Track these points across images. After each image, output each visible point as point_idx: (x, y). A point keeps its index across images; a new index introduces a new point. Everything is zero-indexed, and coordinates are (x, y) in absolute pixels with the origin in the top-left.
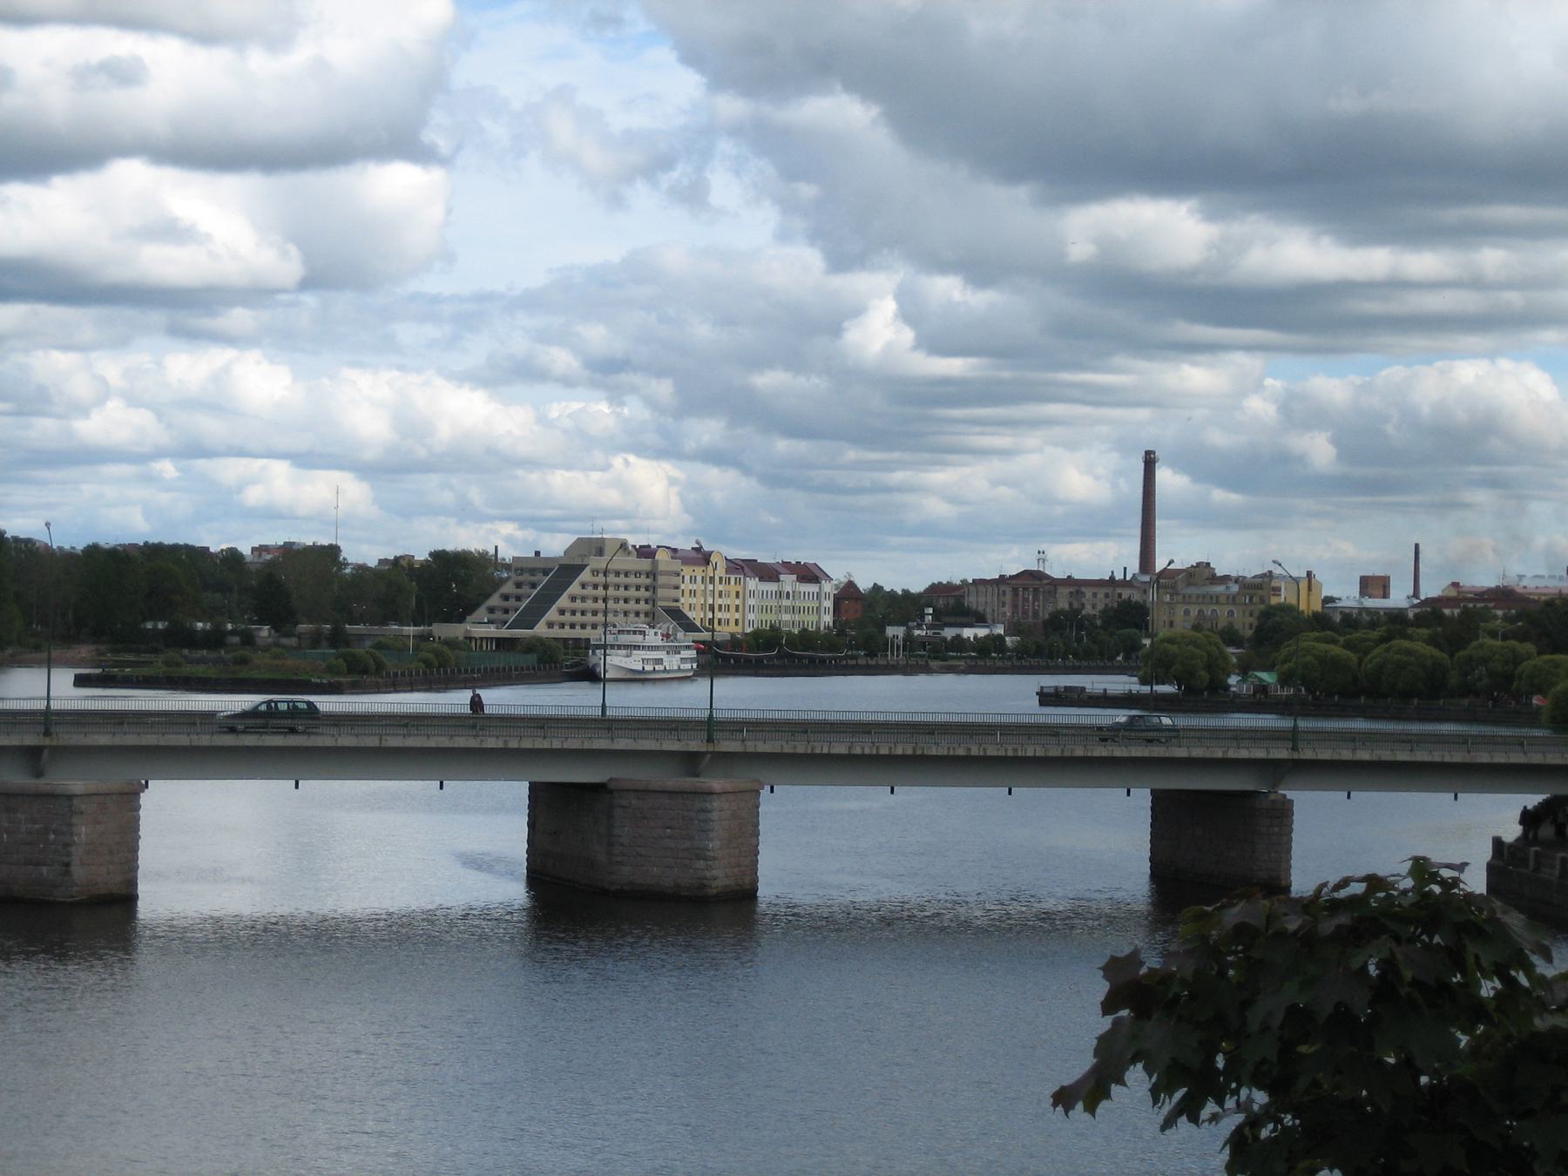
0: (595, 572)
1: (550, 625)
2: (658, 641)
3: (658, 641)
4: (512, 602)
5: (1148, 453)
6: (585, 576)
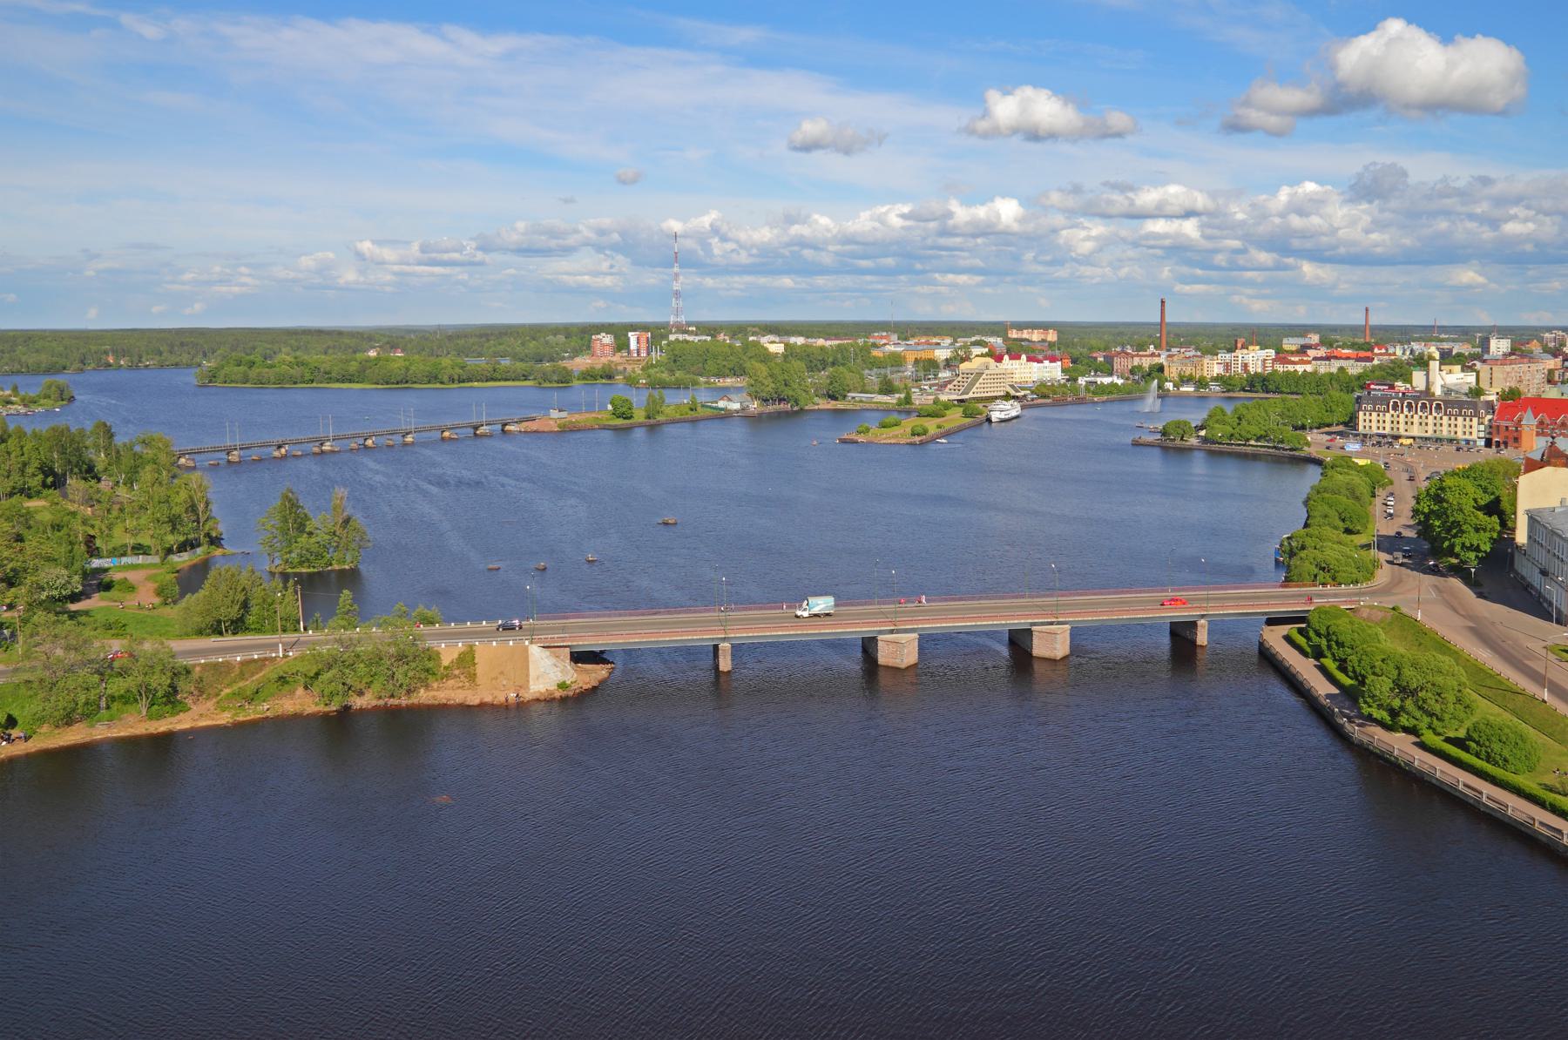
2: (1009, 407)
3: (1009, 407)
4: (965, 379)
6: (984, 376)
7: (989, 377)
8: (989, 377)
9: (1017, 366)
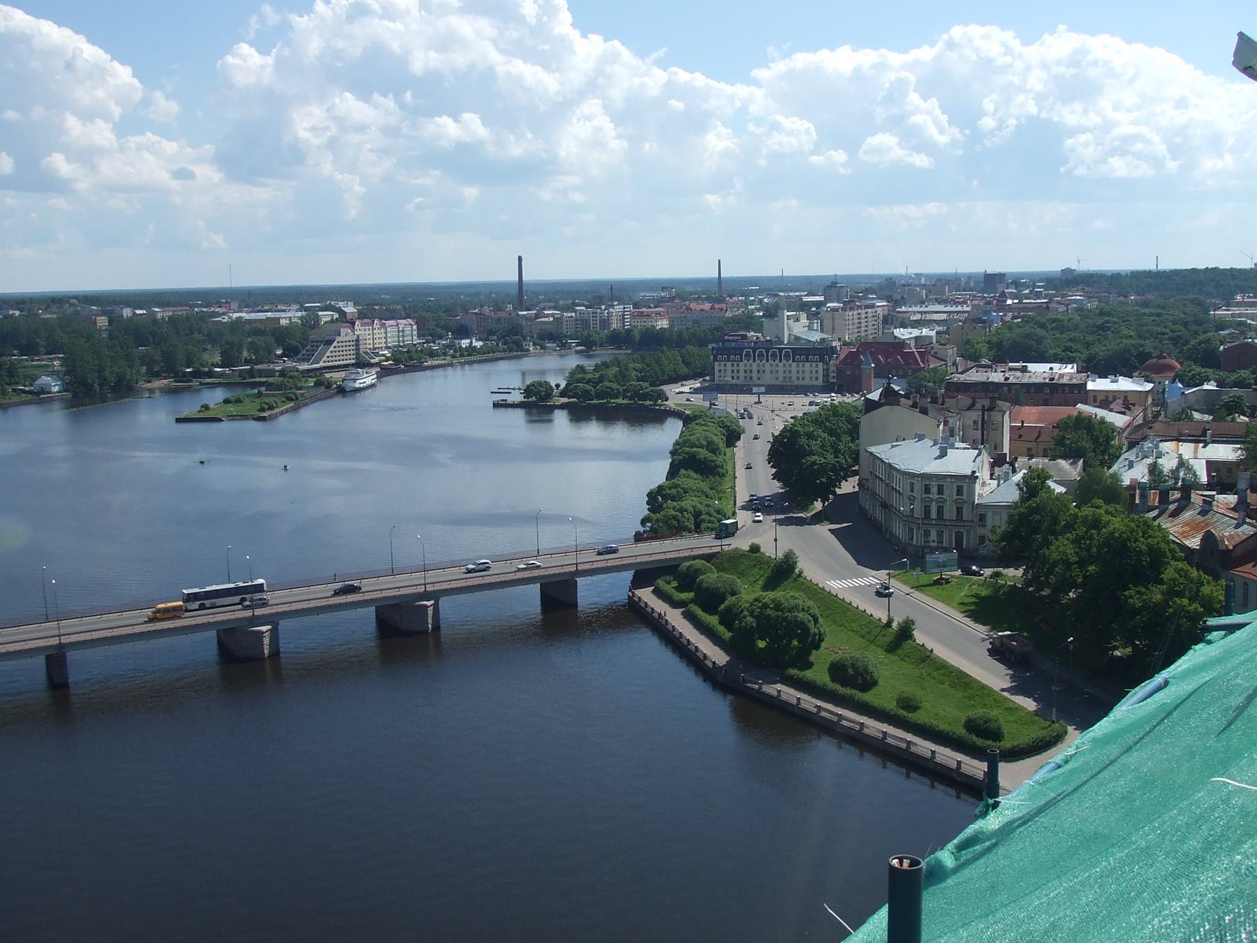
0: (338, 342)
1: (325, 362)
6: (335, 344)
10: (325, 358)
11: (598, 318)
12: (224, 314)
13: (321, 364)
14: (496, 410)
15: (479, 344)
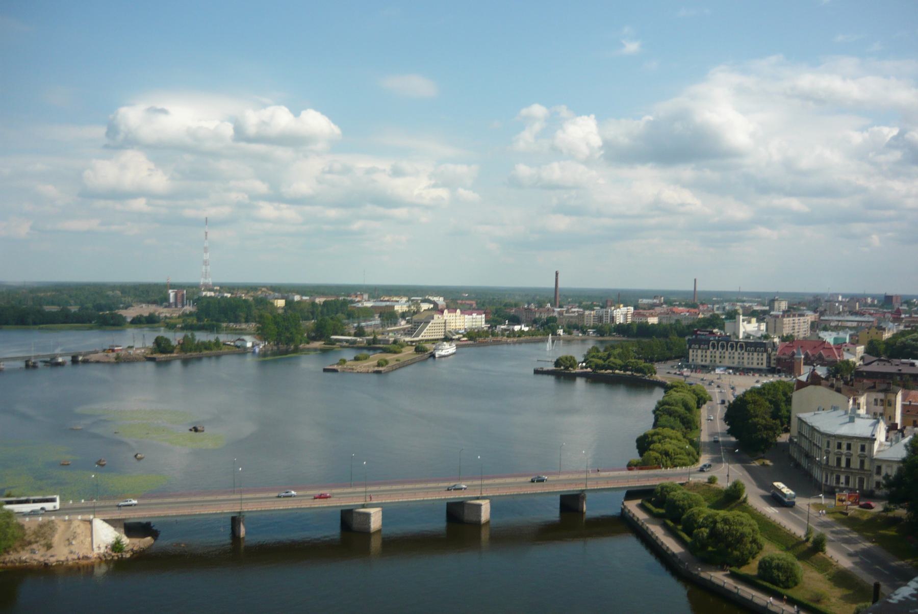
5: (556, 272)
6: (430, 324)
7: (433, 325)
8: (433, 325)
9: (454, 318)
10: (423, 334)
11: (609, 315)
12: (359, 302)
13: (420, 338)
14: (536, 375)
15: (526, 329)
